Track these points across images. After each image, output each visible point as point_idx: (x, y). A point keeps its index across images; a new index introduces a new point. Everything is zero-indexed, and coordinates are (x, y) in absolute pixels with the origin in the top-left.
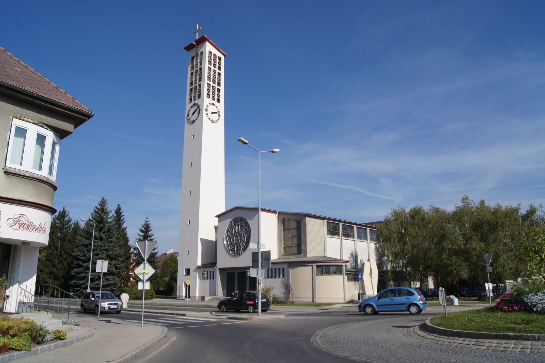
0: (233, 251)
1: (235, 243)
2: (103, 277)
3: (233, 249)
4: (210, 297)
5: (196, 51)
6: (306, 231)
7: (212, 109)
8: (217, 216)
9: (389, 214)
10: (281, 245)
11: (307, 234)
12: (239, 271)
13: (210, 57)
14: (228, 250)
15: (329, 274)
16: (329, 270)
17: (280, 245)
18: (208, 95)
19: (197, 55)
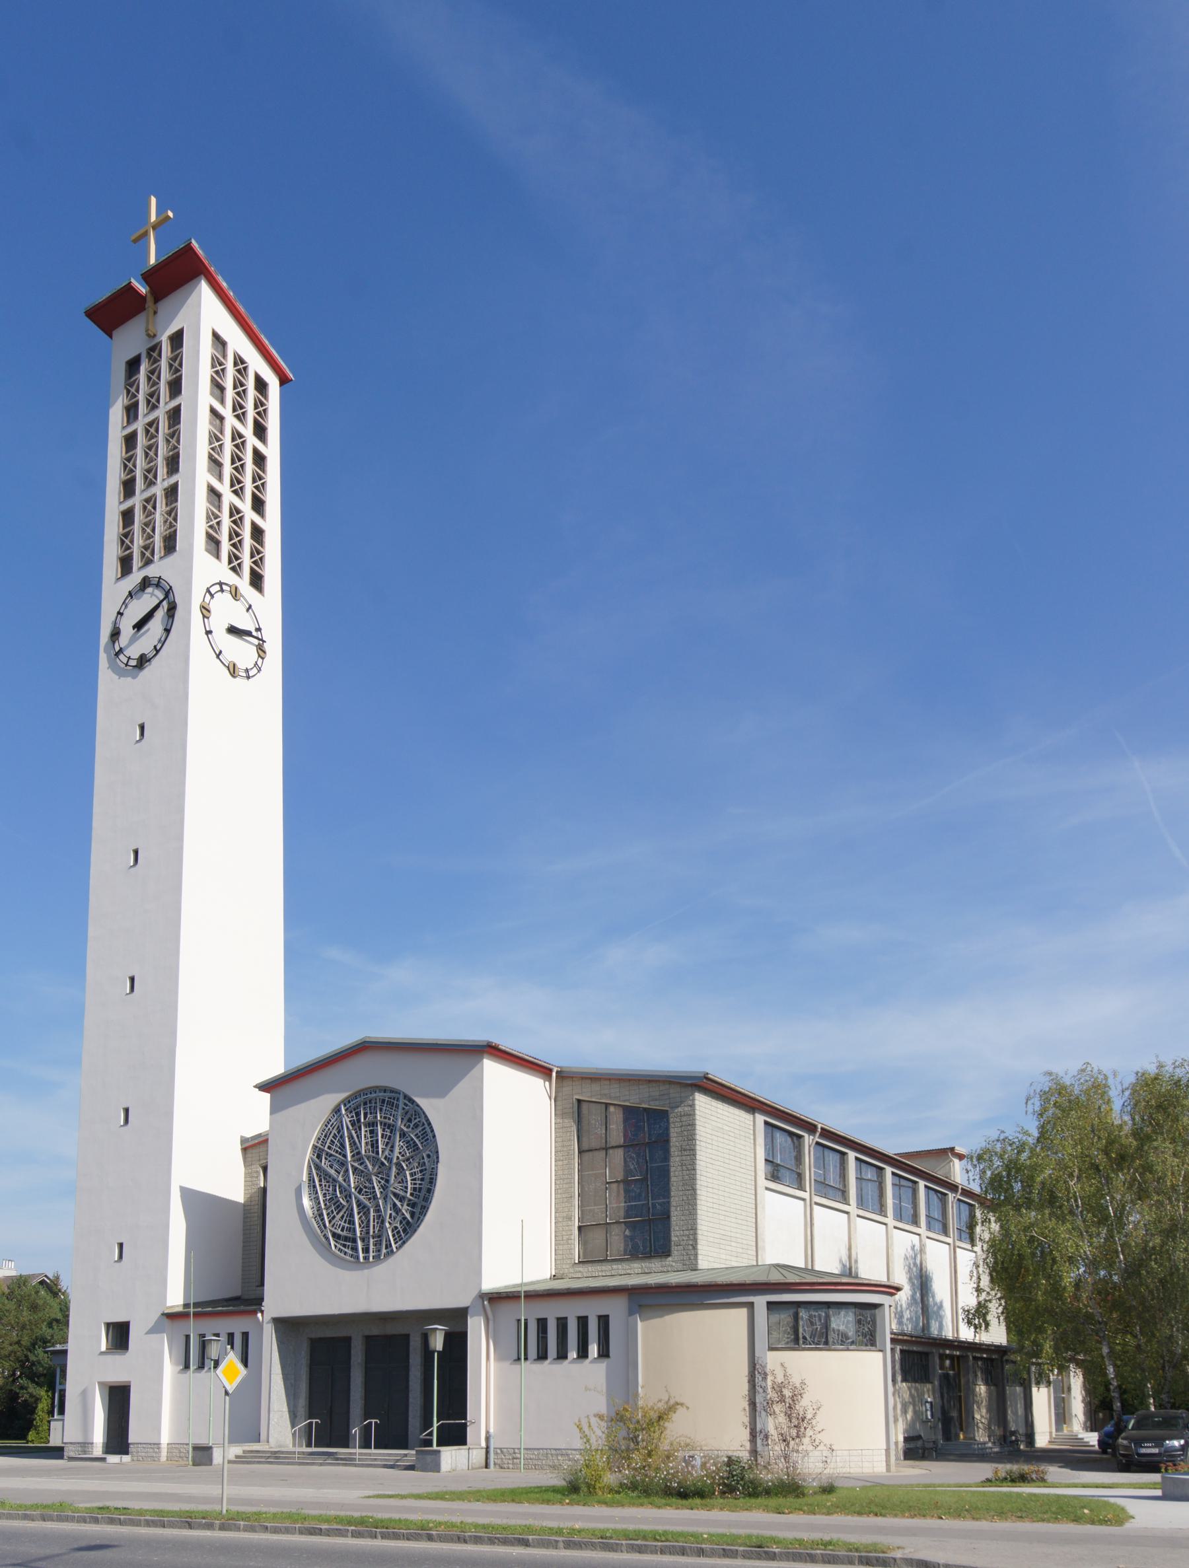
0: (347, 1240)
1: (358, 1206)
3: (344, 1233)
4: (235, 1450)
5: (147, 330)
6: (695, 1155)
7: (226, 611)
8: (265, 1087)
9: (1032, 1094)
10: (570, 1218)
11: (698, 1167)
12: (375, 1331)
14: (321, 1236)
16: (826, 1326)
17: (561, 1218)
18: (213, 543)
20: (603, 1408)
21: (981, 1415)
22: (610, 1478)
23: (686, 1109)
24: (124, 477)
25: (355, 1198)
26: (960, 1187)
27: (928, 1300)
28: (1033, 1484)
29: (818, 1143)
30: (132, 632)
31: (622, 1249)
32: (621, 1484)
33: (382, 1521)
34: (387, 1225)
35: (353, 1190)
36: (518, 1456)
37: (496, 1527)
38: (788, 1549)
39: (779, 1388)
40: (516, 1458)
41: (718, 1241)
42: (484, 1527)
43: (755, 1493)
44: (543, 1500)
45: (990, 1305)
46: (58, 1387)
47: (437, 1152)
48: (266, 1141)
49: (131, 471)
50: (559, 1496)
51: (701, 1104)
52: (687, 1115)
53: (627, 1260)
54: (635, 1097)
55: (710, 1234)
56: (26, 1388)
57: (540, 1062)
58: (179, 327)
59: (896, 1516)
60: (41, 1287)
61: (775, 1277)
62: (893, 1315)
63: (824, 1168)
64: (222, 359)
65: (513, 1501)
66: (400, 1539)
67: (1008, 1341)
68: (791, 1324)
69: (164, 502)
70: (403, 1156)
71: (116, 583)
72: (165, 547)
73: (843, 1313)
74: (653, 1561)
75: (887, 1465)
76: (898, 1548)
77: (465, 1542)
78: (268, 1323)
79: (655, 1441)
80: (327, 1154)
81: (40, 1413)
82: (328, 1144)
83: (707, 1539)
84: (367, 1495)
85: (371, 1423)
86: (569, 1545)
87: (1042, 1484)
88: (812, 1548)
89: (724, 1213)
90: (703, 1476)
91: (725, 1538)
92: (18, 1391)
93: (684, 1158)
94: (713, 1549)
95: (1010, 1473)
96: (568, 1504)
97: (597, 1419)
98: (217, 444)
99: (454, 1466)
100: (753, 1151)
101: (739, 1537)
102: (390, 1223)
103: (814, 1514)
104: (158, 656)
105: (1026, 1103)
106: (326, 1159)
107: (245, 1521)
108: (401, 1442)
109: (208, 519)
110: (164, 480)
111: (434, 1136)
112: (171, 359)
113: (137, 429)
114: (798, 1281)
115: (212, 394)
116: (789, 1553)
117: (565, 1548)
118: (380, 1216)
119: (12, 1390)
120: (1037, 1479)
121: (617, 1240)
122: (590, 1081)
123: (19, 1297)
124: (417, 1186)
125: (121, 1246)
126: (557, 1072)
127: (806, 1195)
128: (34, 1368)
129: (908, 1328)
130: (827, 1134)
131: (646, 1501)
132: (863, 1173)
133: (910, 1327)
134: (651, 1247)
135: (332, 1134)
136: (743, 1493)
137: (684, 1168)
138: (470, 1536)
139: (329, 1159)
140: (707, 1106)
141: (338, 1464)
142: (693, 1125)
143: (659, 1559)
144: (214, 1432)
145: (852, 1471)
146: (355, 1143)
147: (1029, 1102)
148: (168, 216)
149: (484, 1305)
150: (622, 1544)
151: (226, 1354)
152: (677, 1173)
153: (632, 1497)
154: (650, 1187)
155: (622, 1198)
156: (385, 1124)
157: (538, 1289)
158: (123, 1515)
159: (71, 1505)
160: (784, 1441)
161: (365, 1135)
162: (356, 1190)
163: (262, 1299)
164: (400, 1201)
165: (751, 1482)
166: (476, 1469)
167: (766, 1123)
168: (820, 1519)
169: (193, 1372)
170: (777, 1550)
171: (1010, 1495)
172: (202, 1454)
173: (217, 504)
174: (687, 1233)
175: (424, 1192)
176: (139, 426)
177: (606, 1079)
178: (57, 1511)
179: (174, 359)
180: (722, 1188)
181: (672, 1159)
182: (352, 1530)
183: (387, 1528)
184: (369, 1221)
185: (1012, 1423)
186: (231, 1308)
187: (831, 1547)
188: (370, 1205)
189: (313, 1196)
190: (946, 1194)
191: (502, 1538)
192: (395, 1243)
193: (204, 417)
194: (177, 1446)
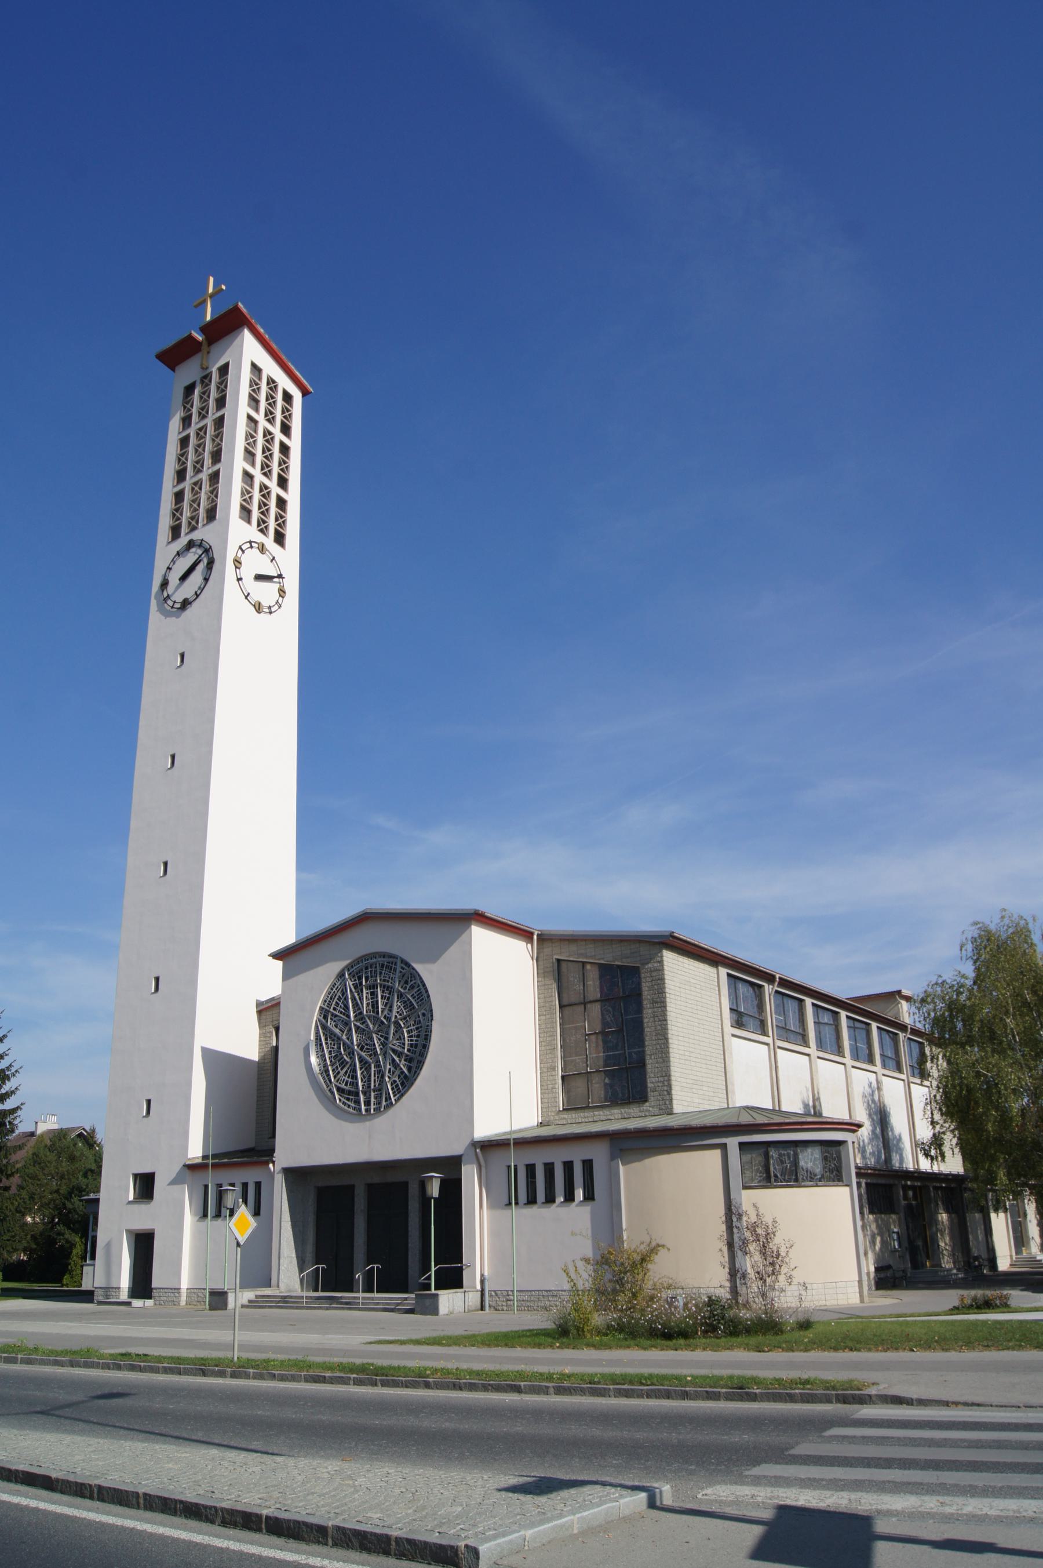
0: (350, 1094)
1: (360, 1062)
2: (681, 1390)
3: (348, 1088)
5: (202, 365)
6: (665, 1007)
7: (255, 563)
8: (278, 956)
9: (964, 940)
10: (553, 1069)
11: (669, 1018)
12: (376, 1179)
13: (252, 383)
15: (796, 1180)
16: (795, 1163)
18: (246, 513)
19: (205, 377)
20: (589, 1253)
21: (944, 1243)
22: (598, 1320)
23: (655, 965)
24: (178, 468)
25: (358, 1055)
26: (909, 1026)
27: (888, 1134)
28: (997, 1311)
29: (777, 992)
30: (178, 582)
31: (602, 1096)
32: (608, 1326)
33: (382, 1368)
34: (387, 1079)
35: (356, 1047)
36: (512, 1297)
37: (490, 1373)
38: (769, 1389)
39: (753, 1228)
40: (510, 1300)
41: (690, 1086)
42: (478, 1374)
43: (736, 1332)
44: (535, 1344)
45: (945, 1137)
46: (91, 1234)
47: (432, 1010)
48: (279, 1003)
49: (184, 463)
50: (550, 1340)
51: (669, 960)
52: (657, 970)
53: (607, 1106)
54: (609, 956)
55: (683, 1080)
56: (63, 1234)
57: (522, 927)
58: (226, 361)
59: (870, 1350)
60: (79, 1139)
61: (745, 1119)
62: (856, 1150)
63: (784, 1014)
64: (258, 381)
65: (506, 1345)
66: (399, 1387)
67: (965, 1169)
68: (763, 1164)
69: (208, 484)
70: (400, 1015)
71: (167, 545)
72: (207, 517)
73: (809, 1150)
74: (640, 1405)
75: (860, 1296)
76: (873, 1384)
77: (461, 1389)
78: (278, 1173)
79: (639, 1283)
80: (333, 1014)
81: (75, 1258)
82: (333, 1006)
83: (691, 1381)
84: (369, 1341)
85: (373, 1267)
86: (560, 1391)
87: (1005, 1310)
88: (791, 1388)
89: (694, 1060)
90: (686, 1317)
91: (708, 1380)
92: (56, 1237)
93: (655, 1009)
94: (696, 1392)
95: (975, 1299)
96: (558, 1347)
97: (584, 1262)
98: (251, 440)
99: (451, 1310)
100: (718, 1001)
101: (721, 1378)
102: (389, 1077)
103: (793, 1351)
104: (198, 600)
105: (961, 950)
106: (331, 1019)
107: (255, 1369)
108: (402, 1287)
109: (243, 494)
110: (209, 468)
111: (428, 996)
112: (219, 383)
113: (190, 434)
114: (766, 1122)
115: (249, 405)
116: (769, 1393)
117: (556, 1394)
118: (380, 1070)
119: (50, 1236)
120: (1001, 1304)
121: (598, 1087)
122: (567, 943)
123: (59, 1149)
124: (414, 1042)
125: (149, 1102)
126: (538, 935)
127: (769, 1040)
128: (70, 1215)
129: (871, 1162)
130: (785, 983)
131: (632, 1342)
132: (820, 1018)
133: (873, 1160)
134: (629, 1094)
135: (337, 997)
136: (725, 1332)
137: (656, 1019)
138: (465, 1384)
139: (334, 1019)
140: (674, 962)
141: (343, 1308)
142: (662, 979)
143: (646, 1403)
144: (227, 1279)
145: (828, 1303)
146: (357, 1004)
147: (963, 949)
148: (222, 289)
149: (476, 1151)
150: (610, 1389)
151: (239, 1207)
152: (650, 1024)
153: (619, 1339)
154: (625, 1037)
155: (601, 1048)
156: (384, 986)
157: (526, 1136)
158: (143, 1362)
159: (97, 1351)
160: (761, 1279)
161: (366, 997)
162: (358, 1047)
163: (273, 1151)
164: (399, 1057)
165: (731, 1321)
166: (472, 1311)
167: (729, 975)
168: (798, 1356)
169: (211, 1221)
170: (758, 1391)
171: (975, 1323)
172: (218, 1299)
173: (249, 483)
174: (661, 1079)
175: (420, 1047)
176: (192, 431)
177: (582, 940)
178: (83, 1357)
179: (221, 383)
180: (692, 1037)
181: (645, 1011)
182: (354, 1378)
183: (387, 1376)
184: (370, 1076)
185: (974, 1250)
186: (245, 1159)
187: (809, 1386)
188: (371, 1061)
189: (320, 1054)
190: (897, 1034)
191: (495, 1385)
192: (394, 1096)
193: (242, 427)
194: (195, 1291)
